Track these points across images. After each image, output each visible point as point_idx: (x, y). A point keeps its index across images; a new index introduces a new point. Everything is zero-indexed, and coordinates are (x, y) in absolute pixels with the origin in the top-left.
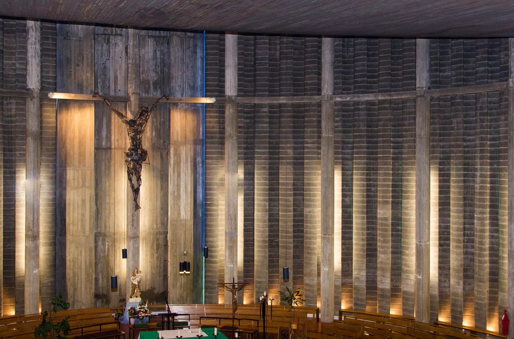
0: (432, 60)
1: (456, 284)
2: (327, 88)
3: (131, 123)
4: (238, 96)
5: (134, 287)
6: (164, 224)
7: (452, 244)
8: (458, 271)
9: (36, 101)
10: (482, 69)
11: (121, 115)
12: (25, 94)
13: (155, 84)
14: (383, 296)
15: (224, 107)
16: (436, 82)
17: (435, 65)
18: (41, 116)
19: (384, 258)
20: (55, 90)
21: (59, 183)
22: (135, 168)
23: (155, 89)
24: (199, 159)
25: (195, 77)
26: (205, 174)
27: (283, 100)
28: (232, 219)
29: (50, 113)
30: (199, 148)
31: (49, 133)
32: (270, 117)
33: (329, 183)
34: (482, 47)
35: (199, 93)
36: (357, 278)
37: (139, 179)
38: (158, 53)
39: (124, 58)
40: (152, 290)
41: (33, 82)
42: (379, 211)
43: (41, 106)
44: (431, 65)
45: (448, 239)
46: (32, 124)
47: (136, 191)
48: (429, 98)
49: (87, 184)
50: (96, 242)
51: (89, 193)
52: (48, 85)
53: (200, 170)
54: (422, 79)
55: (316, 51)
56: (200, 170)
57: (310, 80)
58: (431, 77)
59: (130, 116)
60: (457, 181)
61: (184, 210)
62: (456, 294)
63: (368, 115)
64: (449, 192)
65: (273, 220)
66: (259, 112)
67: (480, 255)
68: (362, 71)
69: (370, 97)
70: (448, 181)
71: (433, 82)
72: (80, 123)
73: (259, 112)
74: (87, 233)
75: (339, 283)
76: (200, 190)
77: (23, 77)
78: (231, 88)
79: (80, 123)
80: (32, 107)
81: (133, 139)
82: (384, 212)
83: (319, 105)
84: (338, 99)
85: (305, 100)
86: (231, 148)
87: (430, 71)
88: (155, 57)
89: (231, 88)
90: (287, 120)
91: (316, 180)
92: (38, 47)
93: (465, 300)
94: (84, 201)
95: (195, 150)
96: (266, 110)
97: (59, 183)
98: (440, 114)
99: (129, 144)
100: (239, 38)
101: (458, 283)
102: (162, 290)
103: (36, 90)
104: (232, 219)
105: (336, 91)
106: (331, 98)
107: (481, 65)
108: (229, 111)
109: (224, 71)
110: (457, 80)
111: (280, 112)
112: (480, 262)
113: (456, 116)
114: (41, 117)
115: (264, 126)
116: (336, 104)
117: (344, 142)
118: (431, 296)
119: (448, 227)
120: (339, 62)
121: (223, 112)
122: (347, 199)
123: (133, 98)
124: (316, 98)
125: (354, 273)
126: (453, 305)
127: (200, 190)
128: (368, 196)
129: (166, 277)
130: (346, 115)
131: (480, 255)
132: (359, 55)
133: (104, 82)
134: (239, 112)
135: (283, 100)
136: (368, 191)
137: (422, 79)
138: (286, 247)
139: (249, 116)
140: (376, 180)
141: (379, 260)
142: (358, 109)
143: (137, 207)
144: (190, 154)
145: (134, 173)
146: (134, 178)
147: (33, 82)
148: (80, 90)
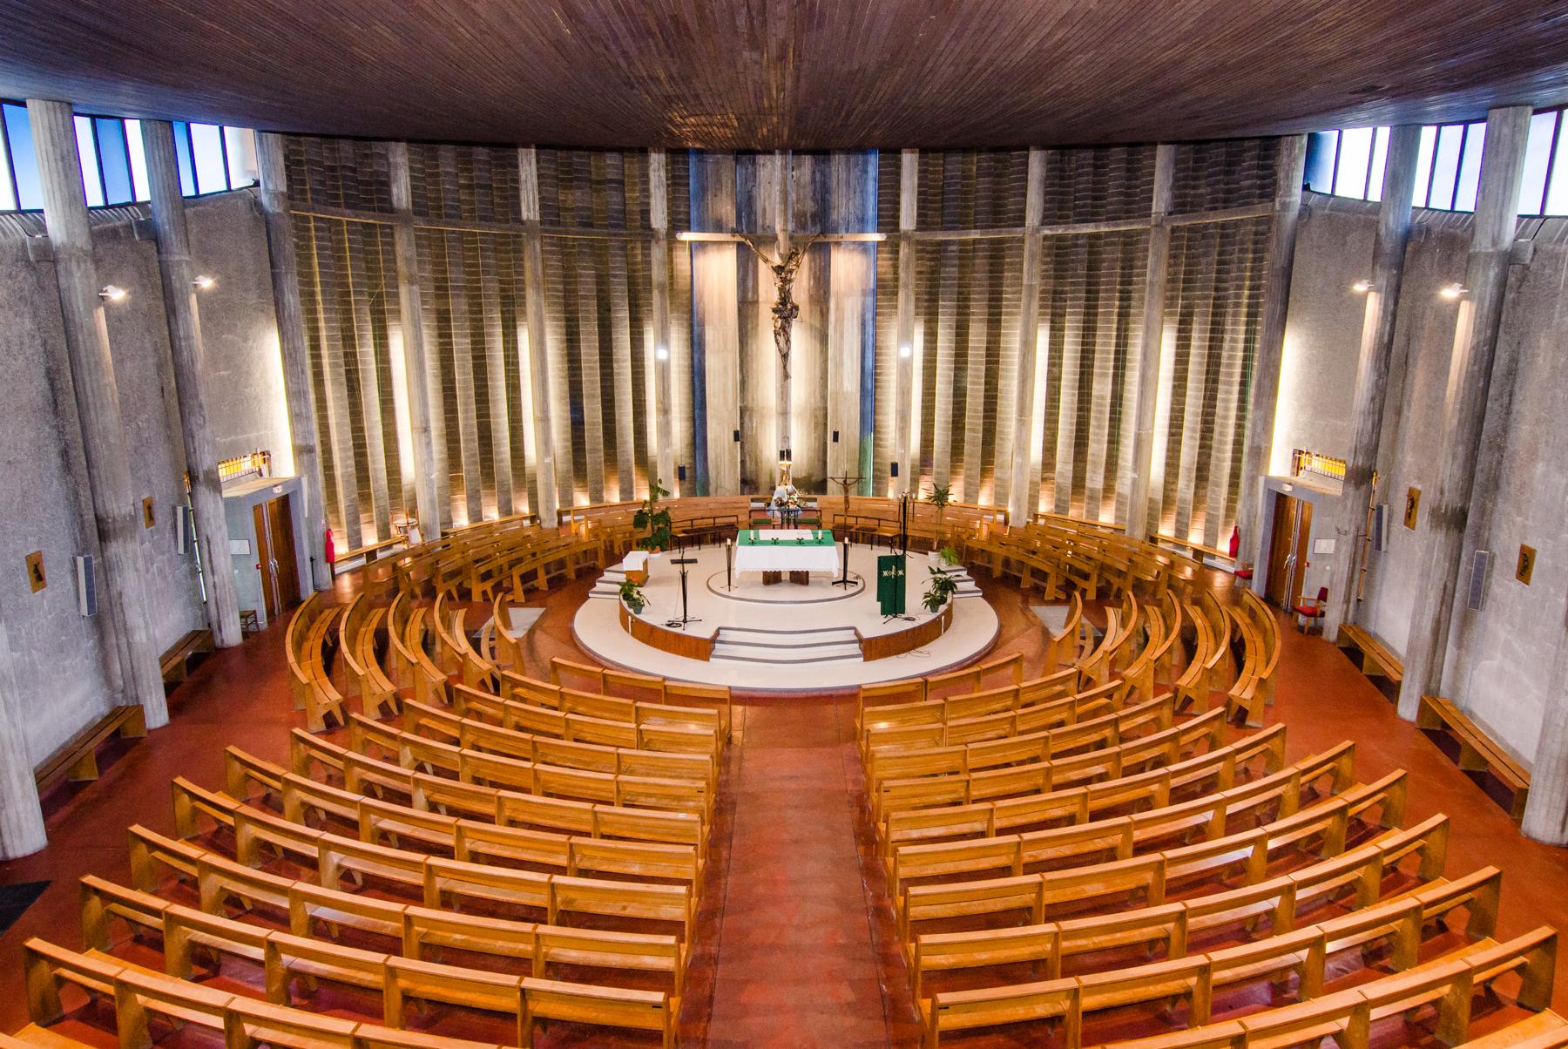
0: (1178, 171)
1: (1185, 487)
2: (1033, 216)
3: (778, 270)
4: (918, 229)
5: (783, 473)
6: (824, 398)
7: (1186, 434)
8: (1189, 470)
9: (664, 243)
10: (1248, 182)
11: (766, 261)
12: (647, 233)
13: (814, 216)
14: (1092, 498)
15: (898, 246)
16: (1180, 205)
17: (1185, 178)
18: (671, 262)
19: (1097, 447)
20: (689, 229)
21: (696, 346)
22: (783, 328)
23: (814, 224)
24: (869, 316)
25: (864, 205)
26: (875, 335)
27: (975, 235)
28: (905, 393)
29: (682, 258)
30: (870, 300)
31: (682, 283)
32: (960, 258)
33: (1028, 346)
34: (1250, 149)
35: (870, 227)
36: (1061, 474)
37: (788, 341)
38: (818, 175)
39: (776, 179)
40: (810, 476)
41: (659, 220)
42: (1095, 385)
43: (670, 250)
44: (1176, 180)
45: (1181, 427)
46: (658, 274)
47: (785, 357)
48: (1168, 228)
49: (729, 346)
50: (742, 417)
51: (733, 357)
52: (678, 222)
53: (870, 329)
54: (1161, 200)
55: (891, 173)
56: (870, 329)
57: (1011, 203)
58: (1175, 196)
59: (777, 261)
60: (1200, 347)
61: (848, 380)
62: (1184, 501)
63: (1090, 253)
64: (1187, 362)
65: (959, 395)
66: (946, 251)
67: (1219, 451)
68: (1085, 190)
69: (1089, 229)
70: (1188, 346)
71: (1176, 205)
72: (716, 271)
73: (946, 251)
74: (730, 406)
75: (1038, 479)
76: (869, 355)
77: (645, 213)
78: (908, 219)
79: (716, 271)
80: (657, 253)
81: (781, 290)
82: (1102, 388)
83: (1022, 240)
84: (1047, 232)
85: (1004, 234)
86: (906, 299)
87: (1174, 187)
88: (813, 181)
89: (908, 219)
90: (981, 262)
91: (1012, 341)
92: (663, 174)
93: (1195, 509)
94: (725, 368)
95: (863, 304)
96: (954, 248)
97: (696, 346)
98: (1186, 247)
99: (776, 297)
100: (1177, 153)
101: (1188, 487)
102: (821, 478)
103: (186, 271)
104: (905, 393)
105: (1047, 220)
106: (1038, 231)
107: (1247, 177)
108: (904, 250)
109: (898, 196)
110: (1212, 201)
111: (974, 250)
112: (1218, 459)
113: (1206, 255)
114: (670, 261)
115: (952, 271)
116: (1046, 238)
117: (1055, 292)
118: (1151, 500)
119: (1182, 410)
120: (1055, 177)
121: (897, 252)
122: (1055, 370)
123: (781, 237)
124: (1017, 232)
125: (1058, 466)
126: (1179, 514)
127: (869, 355)
128: (1082, 366)
129: (825, 463)
130: (1058, 254)
131: (1219, 451)
132: (1083, 167)
133: (749, 216)
134: (918, 251)
135: (975, 235)
136: (1082, 358)
137: (1161, 200)
138: (973, 430)
139: (933, 256)
140: (1094, 344)
141: (1090, 451)
142: (1076, 246)
143: (786, 376)
144: (858, 309)
145: (783, 332)
146: (782, 340)
147: (659, 220)
148: (719, 227)
